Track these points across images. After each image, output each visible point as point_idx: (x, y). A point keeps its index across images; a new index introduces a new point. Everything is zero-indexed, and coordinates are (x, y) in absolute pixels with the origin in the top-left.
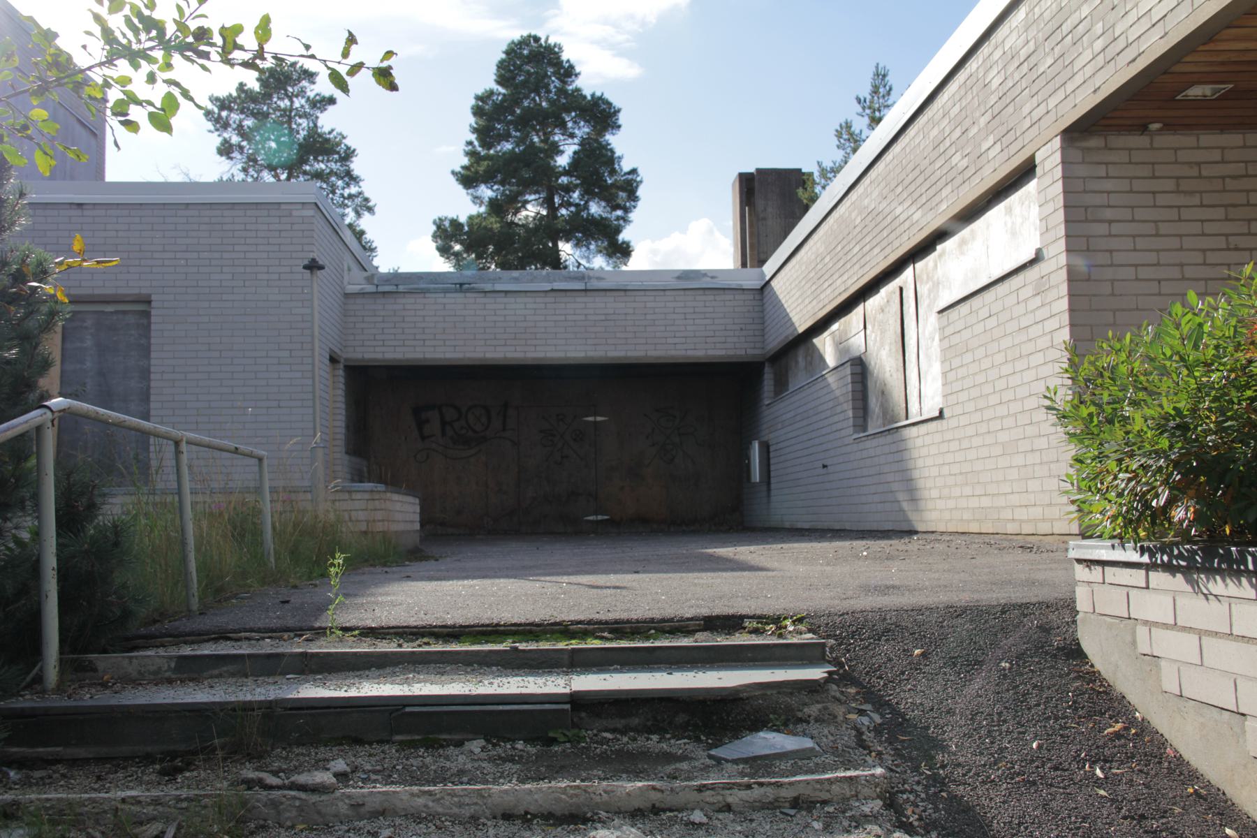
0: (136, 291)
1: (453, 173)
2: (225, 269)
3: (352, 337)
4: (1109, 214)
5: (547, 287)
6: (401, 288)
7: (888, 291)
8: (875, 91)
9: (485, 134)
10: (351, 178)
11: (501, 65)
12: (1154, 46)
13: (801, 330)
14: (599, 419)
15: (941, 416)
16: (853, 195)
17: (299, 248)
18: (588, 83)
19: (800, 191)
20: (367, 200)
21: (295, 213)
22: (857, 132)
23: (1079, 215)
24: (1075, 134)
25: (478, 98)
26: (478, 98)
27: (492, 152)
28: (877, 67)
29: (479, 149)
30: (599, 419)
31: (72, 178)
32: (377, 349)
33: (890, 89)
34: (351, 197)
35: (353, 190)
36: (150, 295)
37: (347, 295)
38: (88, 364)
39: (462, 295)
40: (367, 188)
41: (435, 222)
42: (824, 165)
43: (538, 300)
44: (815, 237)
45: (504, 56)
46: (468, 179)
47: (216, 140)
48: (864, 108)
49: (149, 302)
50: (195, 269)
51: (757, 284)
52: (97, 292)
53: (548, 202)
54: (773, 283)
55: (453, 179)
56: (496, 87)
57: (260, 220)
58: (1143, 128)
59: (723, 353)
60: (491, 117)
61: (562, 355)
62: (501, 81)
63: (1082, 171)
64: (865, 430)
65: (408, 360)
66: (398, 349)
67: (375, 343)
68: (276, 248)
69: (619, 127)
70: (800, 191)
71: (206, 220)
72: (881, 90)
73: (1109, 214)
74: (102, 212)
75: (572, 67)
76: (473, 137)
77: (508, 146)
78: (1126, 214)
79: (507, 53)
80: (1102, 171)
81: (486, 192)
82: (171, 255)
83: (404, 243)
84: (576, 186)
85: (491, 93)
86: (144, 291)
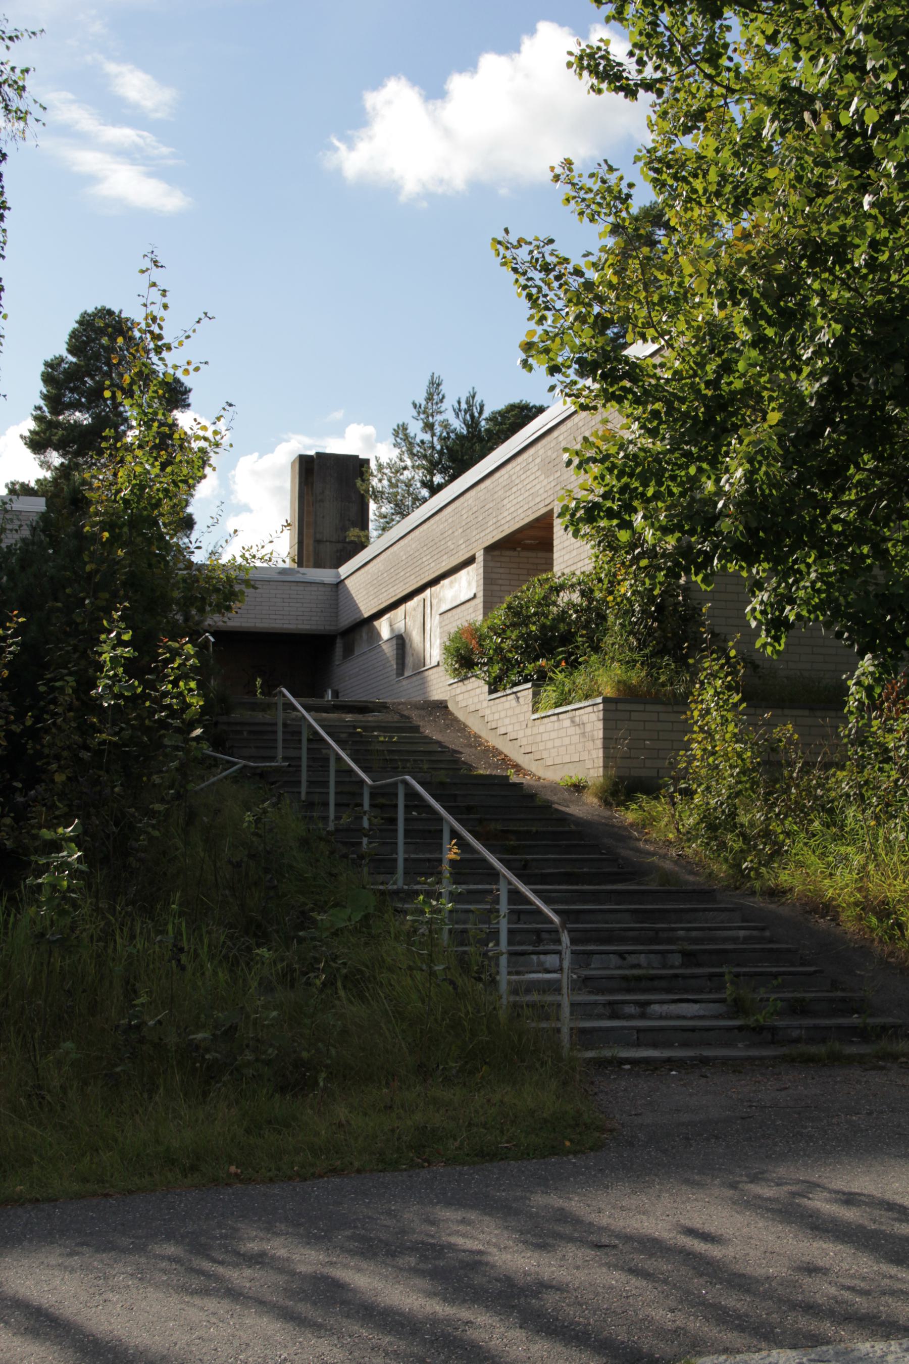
1: (21, 436)
4: (500, 582)
7: (417, 600)
8: (430, 398)
9: (55, 402)
11: (74, 335)
12: (508, 529)
13: (366, 615)
15: (438, 665)
16: (402, 542)
19: (359, 482)
22: (412, 435)
23: (489, 581)
24: (489, 550)
25: (47, 364)
26: (47, 364)
27: (61, 418)
28: (432, 377)
29: (48, 415)
33: (443, 397)
41: (7, 485)
42: (381, 461)
44: (378, 559)
45: (76, 326)
46: (37, 444)
48: (419, 413)
51: (333, 580)
54: (427, 673)
55: (21, 443)
56: (65, 354)
58: (515, 549)
59: (308, 627)
60: (60, 382)
63: (491, 564)
64: (402, 674)
69: (189, 405)
70: (359, 482)
72: (435, 397)
73: (500, 582)
76: (42, 403)
78: (507, 582)
79: (80, 323)
80: (499, 565)
85: (61, 360)
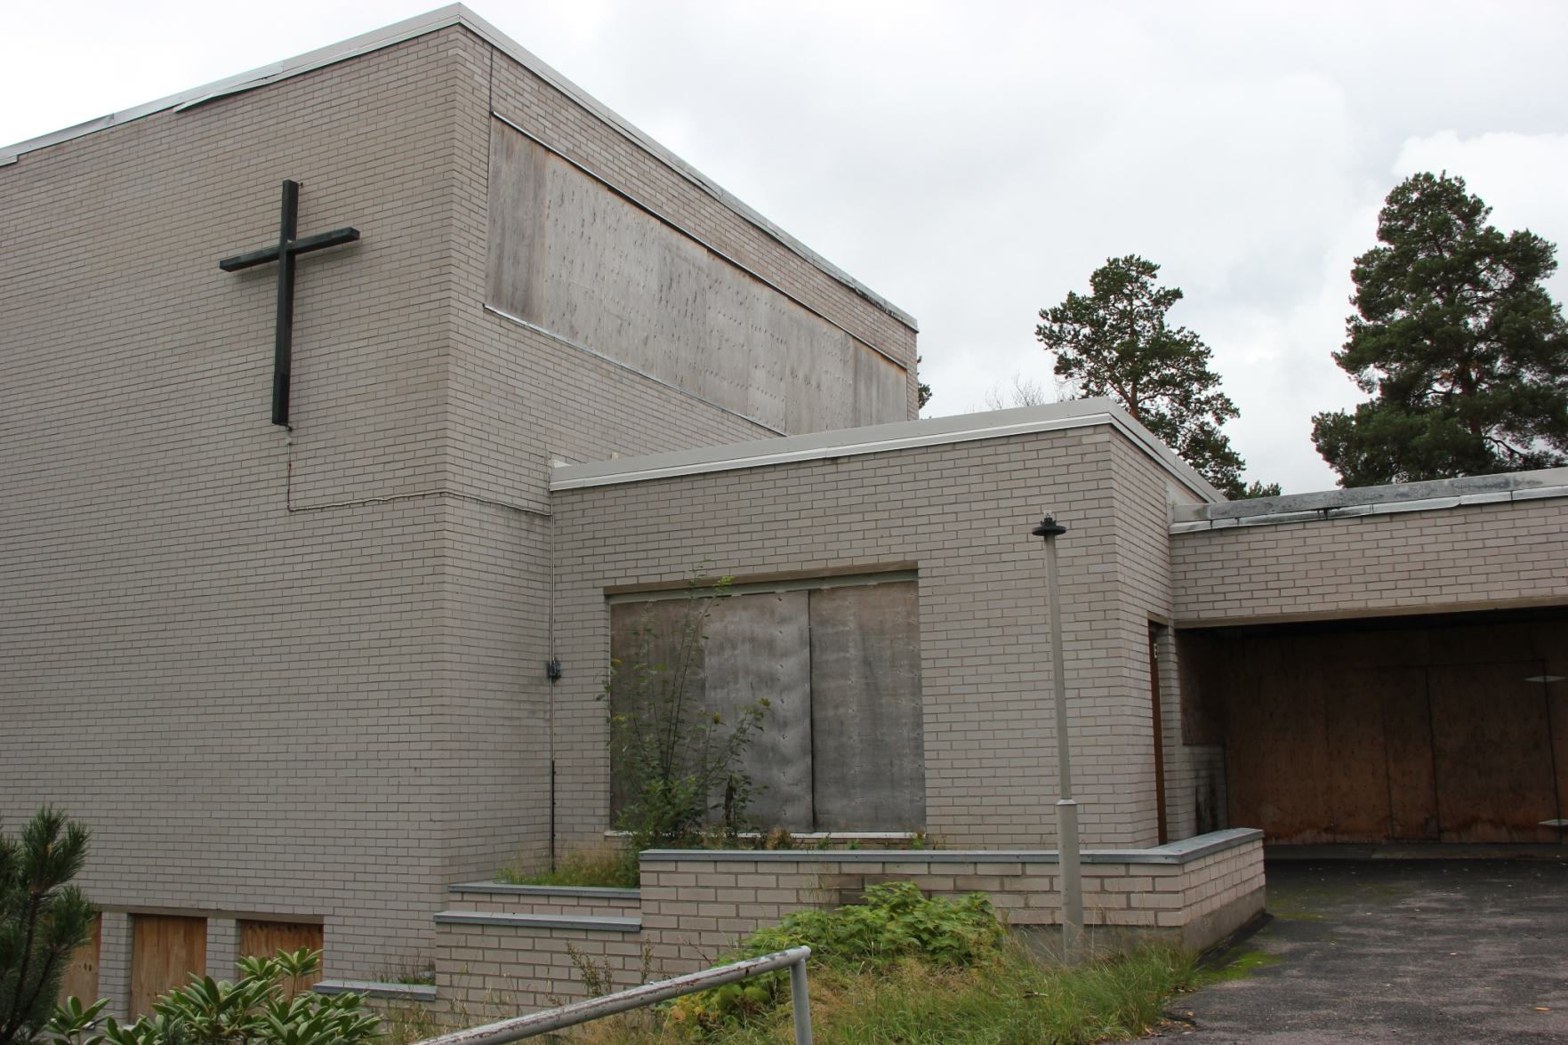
0: (900, 558)
2: (1003, 522)
3: (1182, 592)
5: (1452, 502)
6: (1244, 521)
9: (1368, 303)
10: (1206, 379)
14: (1551, 679)
17: (1093, 485)
18: (1503, 221)
20: (1228, 401)
21: (1085, 440)
25: (1357, 261)
30: (1551, 679)
31: (880, 421)
32: (1217, 605)
34: (1208, 401)
35: (1211, 391)
36: (916, 562)
37: (1172, 537)
38: (852, 651)
39: (1329, 523)
40: (1227, 388)
43: (1439, 522)
46: (1352, 360)
47: (1051, 359)
49: (915, 571)
50: (967, 525)
52: (858, 562)
53: (1461, 378)
55: (1333, 361)
57: (1042, 454)
60: (1375, 282)
61: (1483, 597)
62: (1384, 234)
65: (1258, 618)
66: (1245, 603)
67: (1212, 597)
68: (1065, 488)
71: (977, 461)
74: (858, 466)
75: (1479, 202)
77: (1399, 314)
81: (1375, 373)
82: (938, 510)
83: (1278, 448)
84: (1499, 351)
86: (909, 558)
